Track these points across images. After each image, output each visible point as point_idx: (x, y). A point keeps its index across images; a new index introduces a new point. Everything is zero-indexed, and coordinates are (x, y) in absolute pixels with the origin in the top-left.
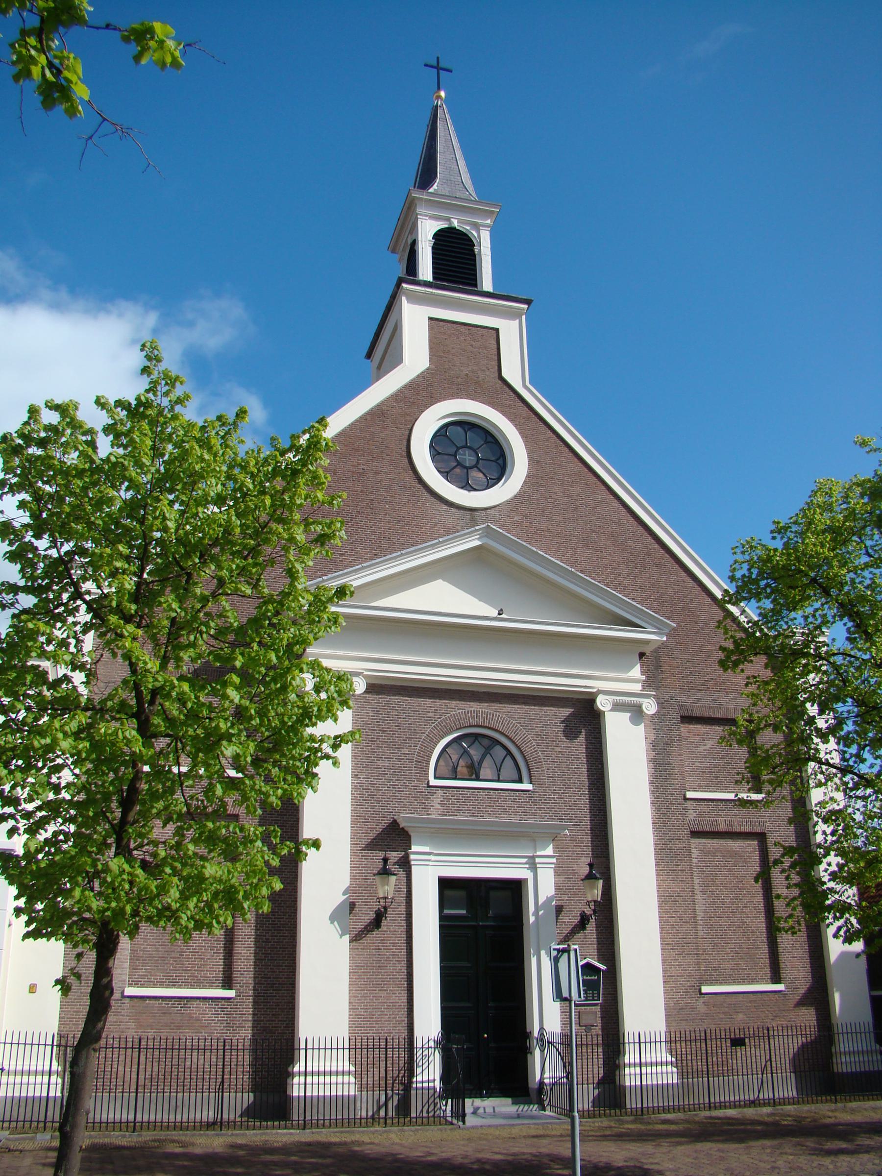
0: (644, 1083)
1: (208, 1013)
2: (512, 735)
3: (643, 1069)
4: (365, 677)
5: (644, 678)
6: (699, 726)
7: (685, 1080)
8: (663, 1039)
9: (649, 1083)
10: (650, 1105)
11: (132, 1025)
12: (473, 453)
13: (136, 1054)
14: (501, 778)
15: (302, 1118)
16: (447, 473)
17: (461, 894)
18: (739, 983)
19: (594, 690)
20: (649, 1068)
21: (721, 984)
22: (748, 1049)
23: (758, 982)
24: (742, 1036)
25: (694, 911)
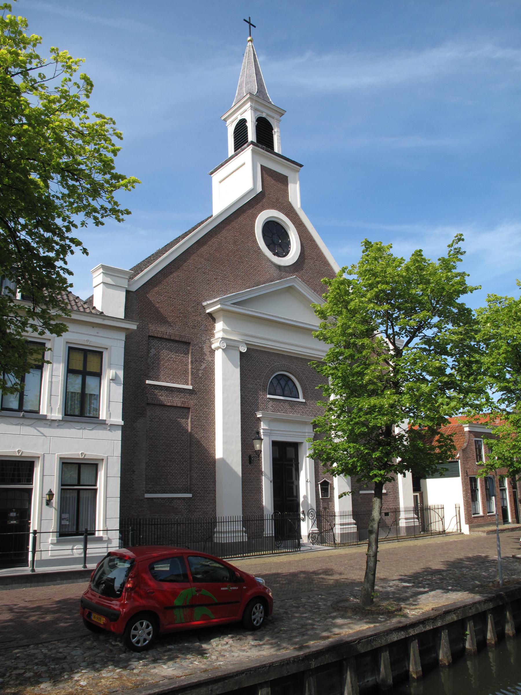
4: (246, 344)
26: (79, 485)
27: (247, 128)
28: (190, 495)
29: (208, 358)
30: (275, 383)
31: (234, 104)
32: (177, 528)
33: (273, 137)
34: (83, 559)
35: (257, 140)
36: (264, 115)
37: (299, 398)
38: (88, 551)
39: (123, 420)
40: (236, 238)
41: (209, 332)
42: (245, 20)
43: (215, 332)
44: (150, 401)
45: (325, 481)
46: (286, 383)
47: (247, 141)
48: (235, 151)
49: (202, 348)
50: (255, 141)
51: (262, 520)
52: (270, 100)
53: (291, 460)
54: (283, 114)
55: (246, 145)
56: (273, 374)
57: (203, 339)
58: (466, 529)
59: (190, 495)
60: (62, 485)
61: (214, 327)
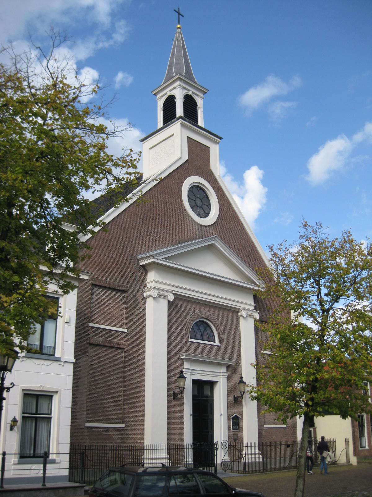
4: (174, 294)
26: (36, 413)
27: (176, 103)
28: (123, 426)
29: (140, 305)
30: (195, 328)
31: (162, 83)
32: (116, 453)
33: (197, 112)
34: (42, 480)
35: (184, 114)
36: (190, 93)
37: (215, 342)
38: (47, 471)
39: (74, 358)
40: (166, 200)
41: (142, 281)
42: (175, 11)
43: (147, 282)
44: (92, 342)
45: (236, 416)
46: (205, 329)
47: (176, 117)
48: (164, 124)
49: (136, 296)
50: (183, 116)
51: (183, 448)
52: (196, 80)
53: (207, 397)
54: (205, 93)
55: (175, 119)
56: (194, 321)
57: (137, 288)
58: (354, 460)
59: (123, 426)
60: (23, 413)
61: (146, 278)
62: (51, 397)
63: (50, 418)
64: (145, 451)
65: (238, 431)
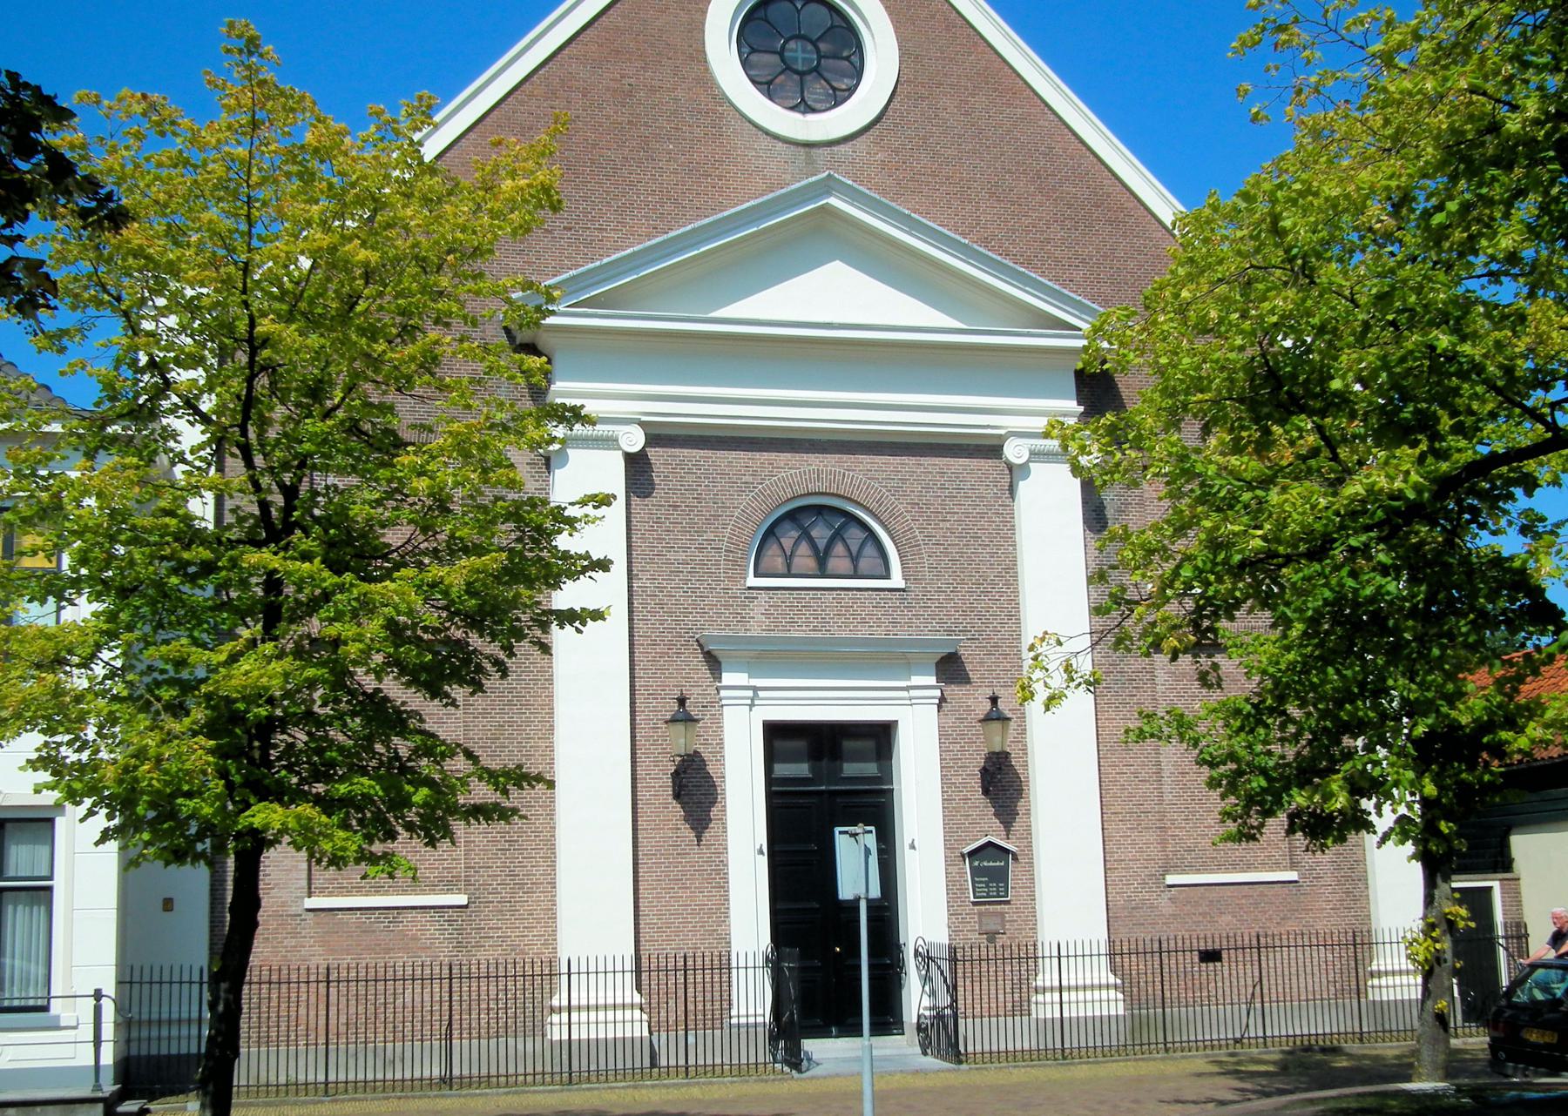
0: (575, 1036)
1: (431, 928)
2: (874, 506)
3: (1065, 995)
4: (642, 424)
5: (1081, 409)
6: (686, 451)
7: (1136, 1012)
8: (1103, 951)
9: (584, 1036)
10: (466, 1072)
11: (319, 949)
12: (810, 47)
13: (323, 990)
14: (829, 571)
15: (565, 1068)
16: (769, 83)
17: (800, 744)
18: (1227, 871)
19: (1002, 432)
20: (1073, 994)
21: (1198, 871)
22: (1226, 968)
23: (1256, 869)
24: (1217, 947)
25: (1158, 764)
37: (887, 576)
59: (462, 899)
62: (51, 821)
63: (50, 889)
64: (734, 972)
65: (1008, 902)
